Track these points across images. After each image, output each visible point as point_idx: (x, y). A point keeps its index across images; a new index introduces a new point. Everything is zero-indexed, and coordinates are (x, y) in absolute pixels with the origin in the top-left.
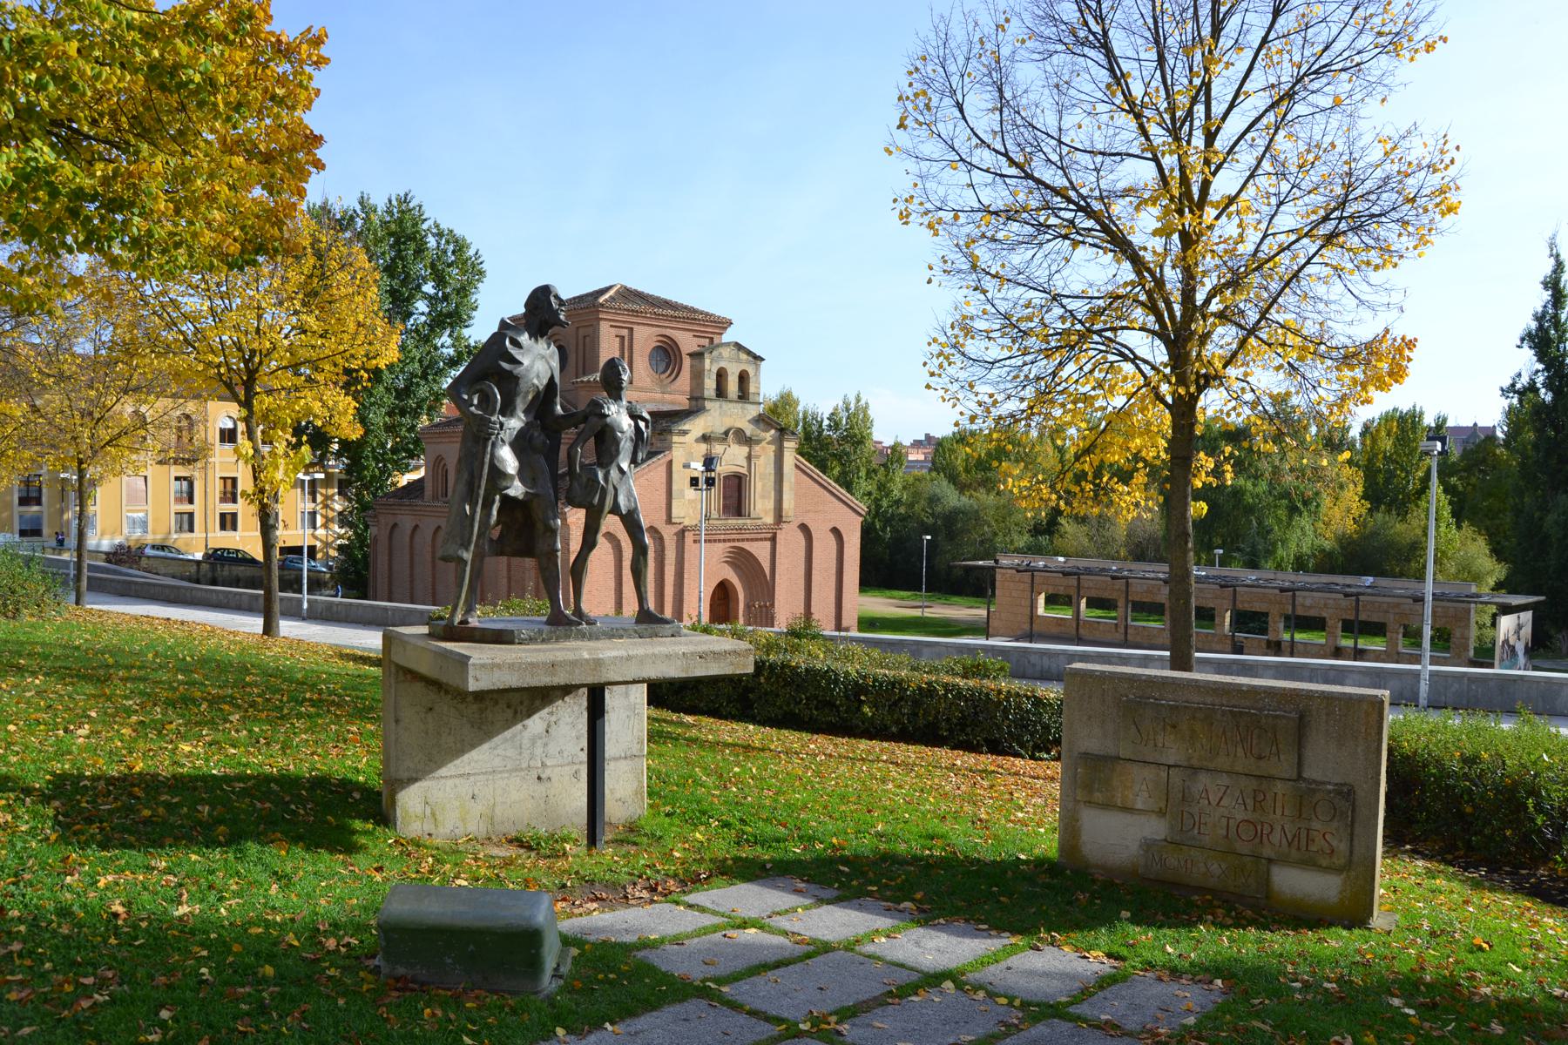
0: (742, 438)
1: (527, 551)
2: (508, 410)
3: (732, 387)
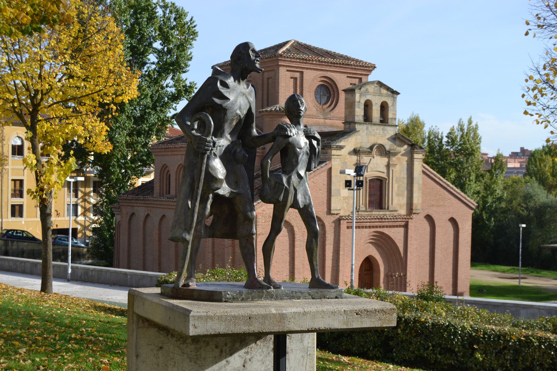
0: (383, 151)
1: (232, 235)
2: (219, 133)
3: (376, 114)
